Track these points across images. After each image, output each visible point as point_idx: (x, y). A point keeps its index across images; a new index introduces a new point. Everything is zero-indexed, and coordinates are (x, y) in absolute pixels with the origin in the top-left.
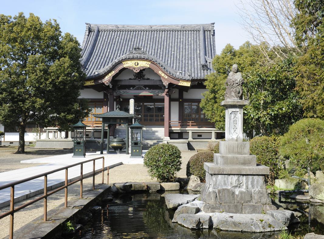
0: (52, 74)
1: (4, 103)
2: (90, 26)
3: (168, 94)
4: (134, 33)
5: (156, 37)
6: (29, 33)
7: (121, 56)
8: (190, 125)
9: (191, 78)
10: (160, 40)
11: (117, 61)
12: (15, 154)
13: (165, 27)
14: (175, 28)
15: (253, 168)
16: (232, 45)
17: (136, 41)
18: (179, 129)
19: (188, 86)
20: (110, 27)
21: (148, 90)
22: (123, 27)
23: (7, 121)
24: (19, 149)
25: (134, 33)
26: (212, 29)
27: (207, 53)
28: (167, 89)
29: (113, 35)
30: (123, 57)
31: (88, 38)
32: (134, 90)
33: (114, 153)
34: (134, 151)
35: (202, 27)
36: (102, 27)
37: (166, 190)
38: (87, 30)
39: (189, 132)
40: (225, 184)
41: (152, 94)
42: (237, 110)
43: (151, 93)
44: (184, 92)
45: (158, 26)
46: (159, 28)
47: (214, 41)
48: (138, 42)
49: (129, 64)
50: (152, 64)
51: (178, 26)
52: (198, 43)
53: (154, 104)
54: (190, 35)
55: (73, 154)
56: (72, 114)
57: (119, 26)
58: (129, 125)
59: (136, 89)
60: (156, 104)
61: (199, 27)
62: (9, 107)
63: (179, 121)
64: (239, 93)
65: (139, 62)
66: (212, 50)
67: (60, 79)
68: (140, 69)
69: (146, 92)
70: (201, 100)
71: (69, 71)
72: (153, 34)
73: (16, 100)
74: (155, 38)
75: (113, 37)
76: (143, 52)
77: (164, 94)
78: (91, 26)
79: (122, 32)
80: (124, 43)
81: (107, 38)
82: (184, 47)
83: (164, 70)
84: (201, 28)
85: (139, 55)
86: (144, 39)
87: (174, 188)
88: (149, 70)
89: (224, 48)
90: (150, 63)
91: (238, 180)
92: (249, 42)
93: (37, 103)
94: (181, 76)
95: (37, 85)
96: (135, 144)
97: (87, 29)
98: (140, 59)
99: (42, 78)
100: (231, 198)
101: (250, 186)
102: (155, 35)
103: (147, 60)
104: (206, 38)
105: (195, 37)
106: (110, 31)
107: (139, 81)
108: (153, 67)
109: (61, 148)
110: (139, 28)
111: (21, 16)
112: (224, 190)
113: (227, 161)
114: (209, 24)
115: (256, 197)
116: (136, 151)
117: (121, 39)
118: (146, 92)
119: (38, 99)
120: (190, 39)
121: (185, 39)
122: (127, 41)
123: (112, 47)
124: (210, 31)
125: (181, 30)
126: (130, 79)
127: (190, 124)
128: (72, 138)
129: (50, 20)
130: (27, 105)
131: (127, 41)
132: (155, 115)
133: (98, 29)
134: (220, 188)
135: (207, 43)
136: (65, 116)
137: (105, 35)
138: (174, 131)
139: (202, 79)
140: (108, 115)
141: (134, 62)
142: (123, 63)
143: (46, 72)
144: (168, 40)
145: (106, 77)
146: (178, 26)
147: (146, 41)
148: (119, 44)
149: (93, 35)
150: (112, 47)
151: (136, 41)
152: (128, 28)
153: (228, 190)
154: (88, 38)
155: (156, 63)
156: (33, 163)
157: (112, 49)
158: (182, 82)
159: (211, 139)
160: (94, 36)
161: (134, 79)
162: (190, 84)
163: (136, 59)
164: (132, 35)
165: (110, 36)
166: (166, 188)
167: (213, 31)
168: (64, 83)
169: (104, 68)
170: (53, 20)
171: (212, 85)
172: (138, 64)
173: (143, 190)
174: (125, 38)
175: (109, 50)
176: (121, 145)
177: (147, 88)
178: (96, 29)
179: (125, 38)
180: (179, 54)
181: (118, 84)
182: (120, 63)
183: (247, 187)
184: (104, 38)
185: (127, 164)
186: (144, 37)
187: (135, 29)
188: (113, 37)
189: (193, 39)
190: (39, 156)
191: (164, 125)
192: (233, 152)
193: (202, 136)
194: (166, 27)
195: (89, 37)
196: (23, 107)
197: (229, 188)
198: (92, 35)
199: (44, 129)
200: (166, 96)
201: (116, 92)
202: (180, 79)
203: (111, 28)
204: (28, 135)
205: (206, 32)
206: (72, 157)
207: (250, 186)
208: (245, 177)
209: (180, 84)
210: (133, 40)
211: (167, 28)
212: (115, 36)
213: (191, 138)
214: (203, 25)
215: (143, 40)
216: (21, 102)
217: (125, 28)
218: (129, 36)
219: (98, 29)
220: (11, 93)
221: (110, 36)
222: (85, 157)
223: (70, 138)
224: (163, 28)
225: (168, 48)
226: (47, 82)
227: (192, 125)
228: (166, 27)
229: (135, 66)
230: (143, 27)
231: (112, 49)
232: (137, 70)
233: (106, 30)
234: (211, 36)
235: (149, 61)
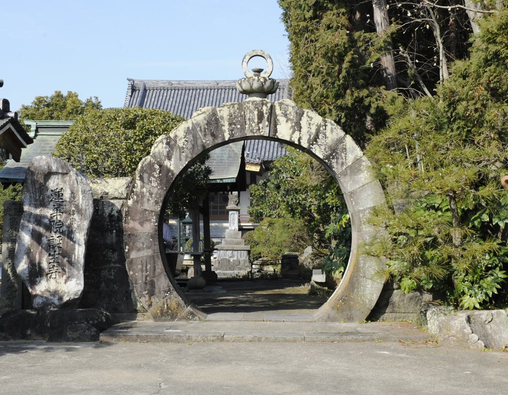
2: (134, 83)
4: (194, 92)
15: (243, 246)
17: (196, 105)
18: (251, 224)
20: (161, 84)
22: (179, 84)
25: (194, 92)
29: (165, 95)
31: (130, 99)
40: (225, 256)
42: (235, 212)
45: (226, 82)
58: (180, 220)
64: (236, 201)
72: (219, 94)
75: (164, 98)
78: (135, 82)
79: (177, 91)
80: (180, 107)
81: (156, 100)
91: (232, 253)
100: (228, 263)
101: (239, 257)
102: (223, 96)
106: (161, 90)
110: (201, 85)
112: (224, 259)
113: (227, 243)
115: (242, 263)
117: (176, 102)
122: (184, 104)
129: (91, 98)
131: (184, 104)
132: (217, 209)
134: (222, 258)
137: (154, 96)
138: (244, 227)
149: (138, 95)
151: (196, 105)
152: (185, 84)
153: (226, 259)
154: (130, 99)
158: (249, 167)
160: (138, 99)
162: (259, 168)
165: (161, 98)
170: (94, 97)
174: (182, 100)
178: (142, 88)
179: (182, 100)
183: (237, 257)
184: (153, 100)
186: (208, 98)
188: (164, 98)
191: (228, 220)
192: (231, 238)
195: (132, 99)
197: (227, 258)
198: (136, 96)
203: (161, 85)
207: (239, 257)
208: (236, 252)
212: (168, 97)
215: (205, 102)
221: (161, 98)
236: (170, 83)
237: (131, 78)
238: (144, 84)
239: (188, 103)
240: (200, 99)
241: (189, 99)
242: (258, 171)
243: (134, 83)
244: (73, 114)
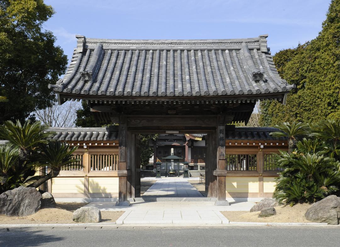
18: (193, 164)
209: (195, 139)
227: (200, 162)
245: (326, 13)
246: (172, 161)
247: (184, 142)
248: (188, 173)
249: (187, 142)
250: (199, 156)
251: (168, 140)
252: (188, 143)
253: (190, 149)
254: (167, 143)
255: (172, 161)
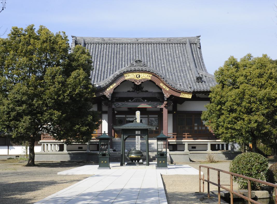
0: (69, 86)
1: (24, 115)
2: (76, 39)
3: (167, 106)
4: (121, 46)
5: (119, 51)
6: (45, 45)
7: (123, 68)
8: (186, 137)
9: (192, 90)
10: (148, 52)
11: (119, 74)
12: (26, 167)
13: (151, 40)
14: (161, 41)
16: (235, 57)
18: (175, 141)
19: (189, 98)
21: (146, 102)
22: (109, 40)
23: (28, 133)
24: (29, 162)
26: (198, 42)
27: (197, 65)
28: (166, 101)
29: (100, 47)
30: (124, 69)
32: (133, 102)
33: (134, 164)
34: (160, 162)
35: (188, 40)
36: (88, 40)
37: (258, 198)
38: (74, 43)
39: (185, 144)
41: (150, 106)
43: (149, 105)
44: (177, 104)
45: (144, 39)
46: (145, 40)
47: (201, 54)
48: (126, 54)
49: (130, 77)
50: (154, 77)
51: (164, 39)
52: (186, 55)
53: (148, 116)
54: (177, 48)
55: (98, 166)
56: (86, 126)
57: (105, 39)
59: (134, 102)
60: (150, 116)
61: (185, 40)
62: (30, 119)
63: (173, 133)
65: (140, 74)
66: (201, 62)
67: (77, 91)
68: (142, 81)
69: (145, 104)
70: (202, 112)
71: (84, 83)
73: (35, 112)
74: (142, 51)
75: (100, 49)
76: (144, 65)
77: (162, 106)
78: (77, 38)
80: (113, 55)
82: (173, 60)
83: (166, 82)
84: (187, 41)
85: (140, 68)
86: (132, 52)
87: (265, 196)
88: (151, 82)
89: (227, 60)
90: (151, 75)
92: (251, 54)
93: (55, 114)
94: (182, 88)
95: (56, 97)
96: (161, 156)
97: (73, 41)
98: (142, 72)
99: (60, 91)
103: (149, 73)
104: (193, 51)
105: (182, 50)
107: (138, 93)
108: (153, 79)
109: (59, 160)
110: (125, 41)
111: (31, 29)
114: (194, 37)
116: (162, 162)
118: (144, 104)
119: (56, 112)
120: (177, 52)
121: (172, 52)
122: (115, 54)
123: (101, 59)
124: (196, 44)
125: (167, 43)
126: (129, 91)
127: (186, 136)
128: (68, 151)
130: (45, 117)
131: (115, 54)
133: (85, 41)
135: (194, 56)
136: (79, 128)
137: (92, 48)
138: (170, 143)
139: (199, 91)
140: (135, 127)
141: (135, 74)
142: (125, 75)
143: (63, 84)
144: (156, 52)
145: (108, 90)
146: (164, 39)
147: (134, 54)
148: (107, 57)
150: (101, 59)
155: (158, 75)
156: (69, 174)
157: (101, 62)
159: (206, 150)
161: (133, 91)
163: (138, 72)
164: (118, 47)
165: (97, 49)
166: (259, 196)
167: (199, 44)
168: (80, 95)
169: (104, 80)
171: (218, 97)
172: (139, 76)
173: (239, 198)
174: (113, 51)
175: (98, 63)
176: (140, 157)
177: (146, 101)
179: (113, 51)
180: (169, 67)
181: (116, 96)
182: (122, 75)
185: (166, 174)
187: (121, 41)
188: (100, 49)
189: (180, 51)
190: (67, 168)
193: (196, 148)
194: (152, 40)
196: (41, 119)
199: (40, 142)
200: (165, 108)
201: (115, 105)
202: (181, 91)
203: (97, 41)
204: (14, 148)
205: (192, 44)
206: (98, 169)
209: (181, 96)
210: (121, 52)
211: (153, 41)
212: (102, 49)
213: (187, 150)
214: (189, 38)
216: (39, 114)
217: (112, 41)
218: (116, 48)
219: (85, 41)
220: (31, 105)
221: (97, 49)
222: (110, 169)
223: (65, 151)
224: (149, 40)
225: (157, 60)
226: (65, 95)
227: (188, 137)
228: (152, 40)
229: (136, 78)
230: (129, 40)
231: (101, 62)
232: (139, 82)
233: (103, 43)
234: (198, 49)
235: (151, 73)
236: (103, 39)
237: (74, 35)
238: (84, 39)
239: (118, 53)
240: (126, 50)
241: (118, 50)
242: (191, 98)
243: (76, 39)
244: (47, 42)
245: (206, 68)
246: (137, 132)
247: (161, 102)
248: (166, 157)
249: (165, 102)
250: (187, 128)
251: (132, 99)
252: (166, 104)
253: (171, 115)
254: (131, 104)
255: (137, 132)
